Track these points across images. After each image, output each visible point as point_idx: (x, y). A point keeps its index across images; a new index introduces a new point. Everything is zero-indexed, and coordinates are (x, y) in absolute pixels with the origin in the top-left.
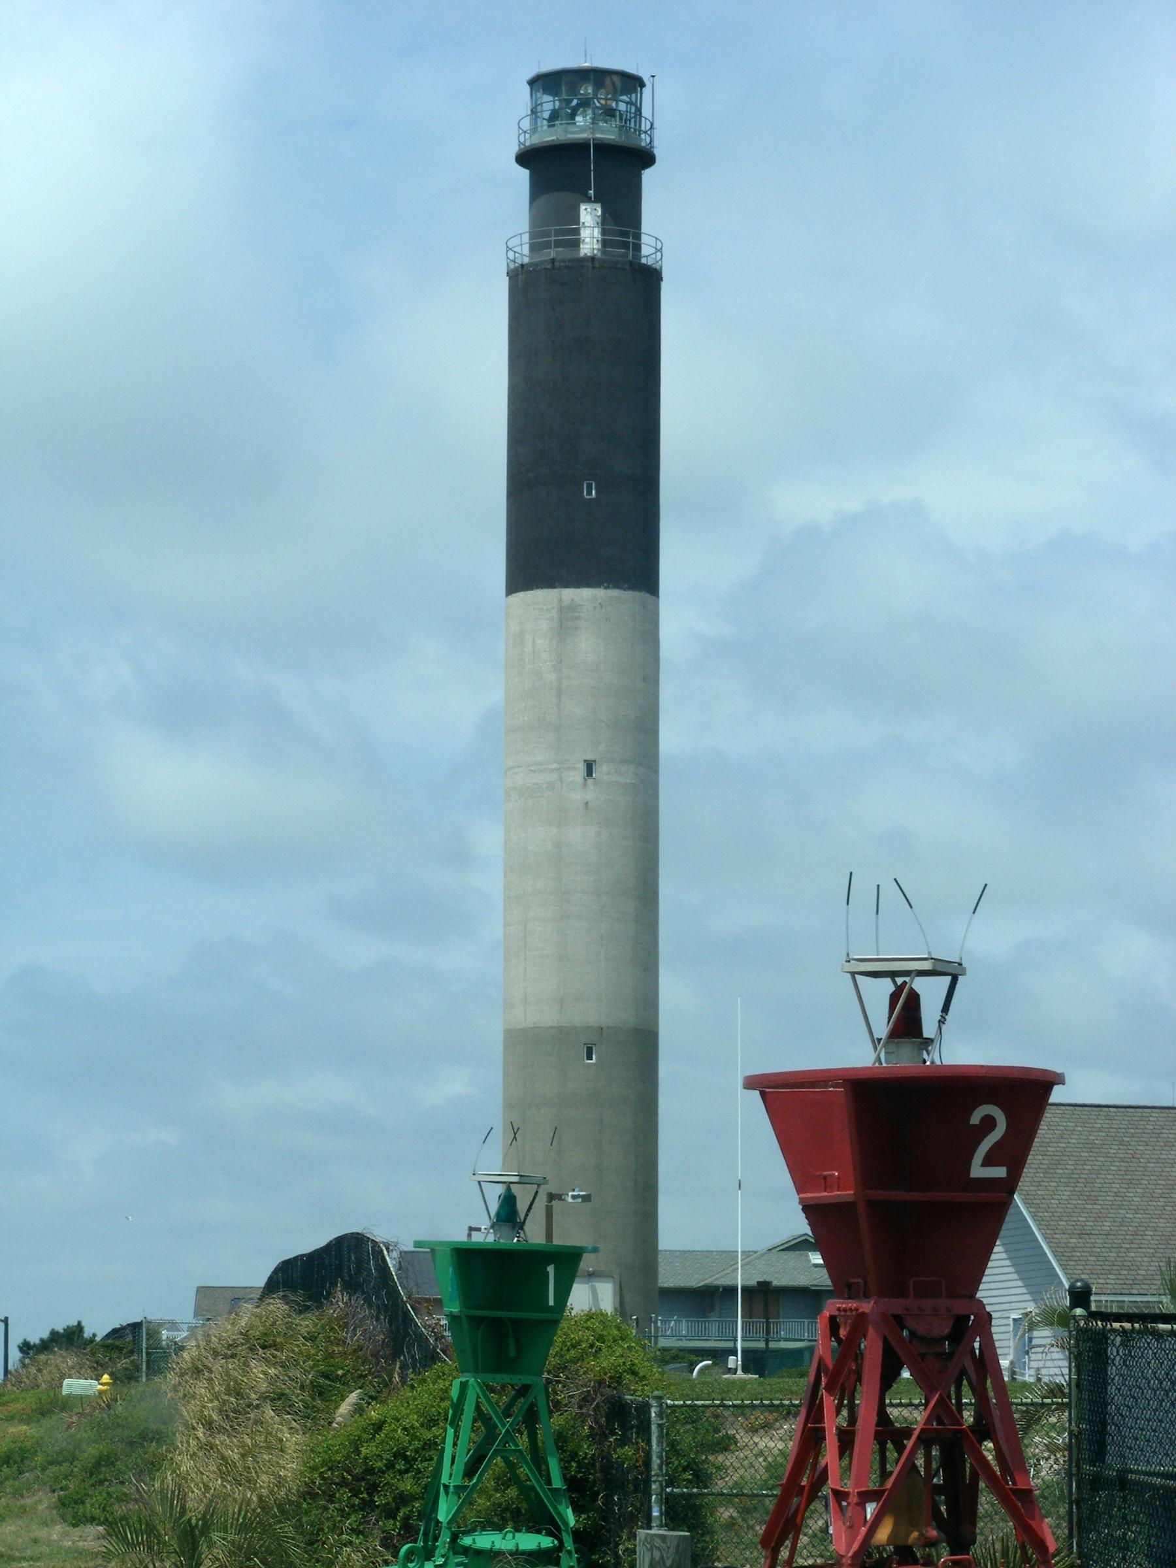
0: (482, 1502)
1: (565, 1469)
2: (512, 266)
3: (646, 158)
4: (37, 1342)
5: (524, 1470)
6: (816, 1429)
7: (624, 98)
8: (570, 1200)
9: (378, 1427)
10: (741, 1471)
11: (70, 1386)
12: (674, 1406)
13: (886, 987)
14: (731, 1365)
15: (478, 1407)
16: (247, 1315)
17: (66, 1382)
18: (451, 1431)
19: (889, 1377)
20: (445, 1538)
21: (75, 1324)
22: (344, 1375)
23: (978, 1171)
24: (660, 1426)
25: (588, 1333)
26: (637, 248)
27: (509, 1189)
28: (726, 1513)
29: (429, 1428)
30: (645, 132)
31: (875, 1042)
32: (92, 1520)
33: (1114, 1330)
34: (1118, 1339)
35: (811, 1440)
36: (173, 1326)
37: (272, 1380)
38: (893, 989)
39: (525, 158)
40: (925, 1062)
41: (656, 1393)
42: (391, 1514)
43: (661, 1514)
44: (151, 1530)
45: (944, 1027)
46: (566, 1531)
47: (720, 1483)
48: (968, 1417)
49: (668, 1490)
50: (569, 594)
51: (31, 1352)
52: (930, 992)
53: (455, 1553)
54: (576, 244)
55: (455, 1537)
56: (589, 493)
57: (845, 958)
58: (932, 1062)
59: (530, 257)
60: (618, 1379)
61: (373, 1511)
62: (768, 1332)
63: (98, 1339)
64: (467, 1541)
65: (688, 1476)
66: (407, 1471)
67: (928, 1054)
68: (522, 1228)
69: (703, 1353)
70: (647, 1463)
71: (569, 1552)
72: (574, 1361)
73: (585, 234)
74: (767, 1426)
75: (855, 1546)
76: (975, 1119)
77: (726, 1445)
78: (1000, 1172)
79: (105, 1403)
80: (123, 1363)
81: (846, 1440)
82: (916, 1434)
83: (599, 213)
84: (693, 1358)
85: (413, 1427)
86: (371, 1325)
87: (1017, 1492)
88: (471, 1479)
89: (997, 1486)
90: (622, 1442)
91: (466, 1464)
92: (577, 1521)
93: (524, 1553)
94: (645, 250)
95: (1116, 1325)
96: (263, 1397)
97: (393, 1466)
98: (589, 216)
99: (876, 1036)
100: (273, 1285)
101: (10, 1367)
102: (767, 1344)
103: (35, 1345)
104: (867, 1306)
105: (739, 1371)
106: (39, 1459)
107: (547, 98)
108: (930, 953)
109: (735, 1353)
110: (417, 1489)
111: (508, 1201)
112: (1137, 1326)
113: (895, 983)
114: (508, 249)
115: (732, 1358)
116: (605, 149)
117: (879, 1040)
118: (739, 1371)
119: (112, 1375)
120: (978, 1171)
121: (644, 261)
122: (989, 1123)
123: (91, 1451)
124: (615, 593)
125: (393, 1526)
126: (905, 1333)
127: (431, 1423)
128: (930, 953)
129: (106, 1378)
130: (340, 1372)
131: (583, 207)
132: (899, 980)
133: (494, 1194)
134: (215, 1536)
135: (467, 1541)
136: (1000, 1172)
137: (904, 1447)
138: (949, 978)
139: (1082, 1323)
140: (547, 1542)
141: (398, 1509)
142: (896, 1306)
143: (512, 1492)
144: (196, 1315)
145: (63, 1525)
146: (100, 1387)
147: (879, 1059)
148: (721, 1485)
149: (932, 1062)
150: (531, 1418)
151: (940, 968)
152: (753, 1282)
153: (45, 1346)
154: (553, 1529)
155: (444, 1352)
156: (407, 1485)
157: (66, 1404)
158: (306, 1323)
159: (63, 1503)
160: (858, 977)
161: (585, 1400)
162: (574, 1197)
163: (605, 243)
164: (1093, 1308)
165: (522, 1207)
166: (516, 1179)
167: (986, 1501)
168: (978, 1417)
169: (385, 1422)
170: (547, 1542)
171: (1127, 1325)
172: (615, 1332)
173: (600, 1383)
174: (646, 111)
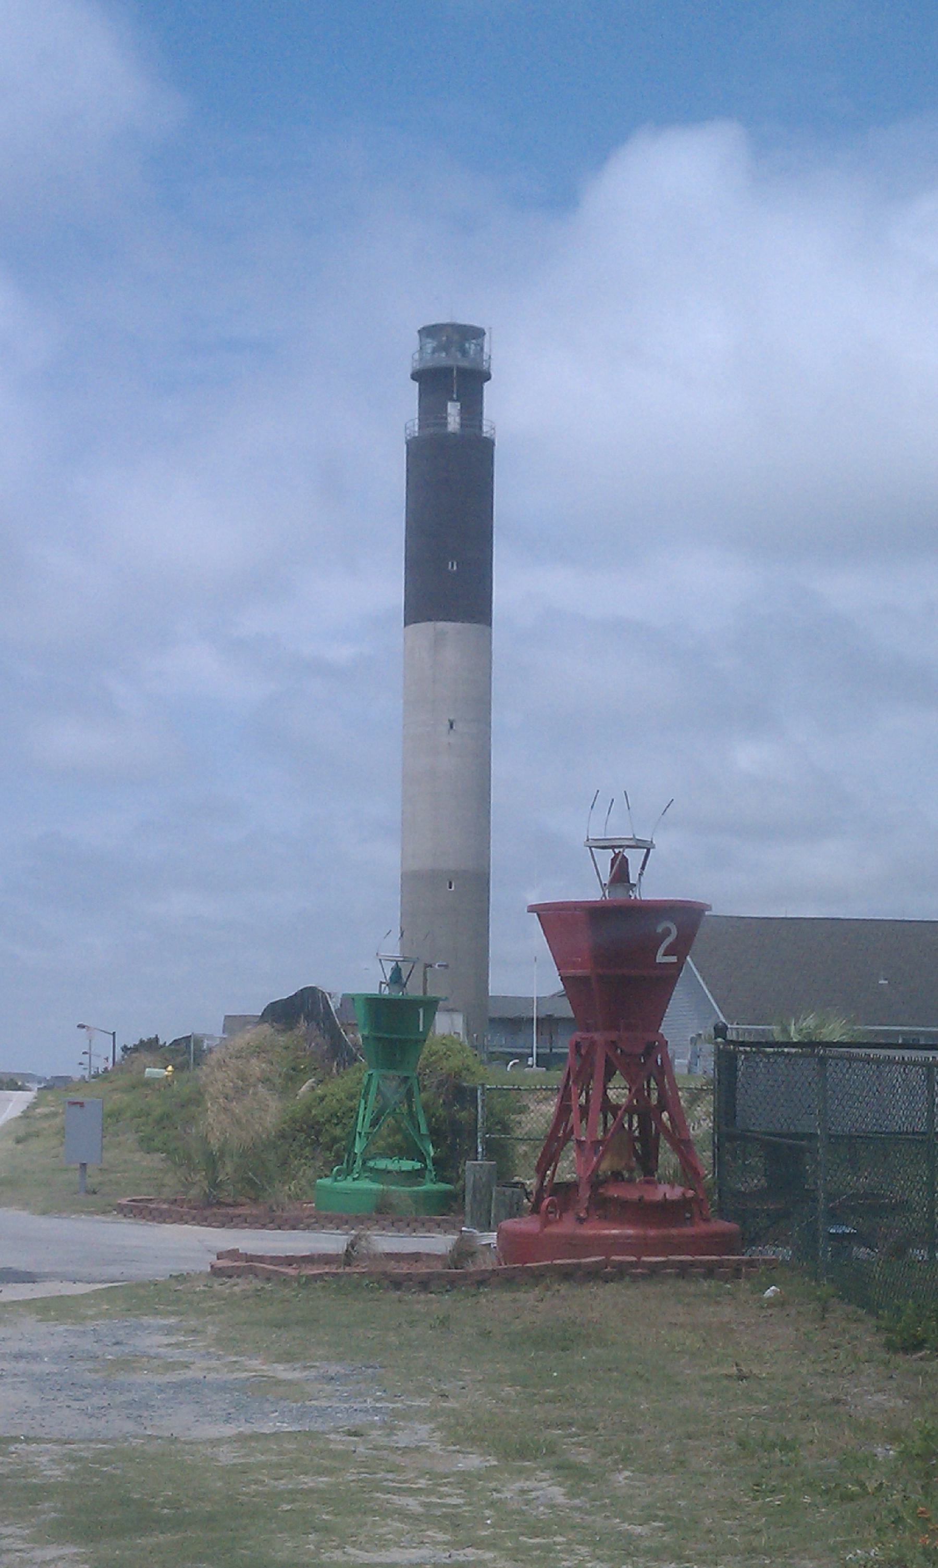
0: (381, 1143)
1: (429, 1124)
2: (408, 438)
3: (488, 377)
4: (132, 1046)
5: (405, 1124)
6: (568, 1105)
7: (474, 341)
8: (436, 967)
9: (322, 1099)
10: (529, 1125)
11: (149, 1072)
12: (491, 1089)
13: (610, 854)
14: (530, 1063)
15: (378, 1088)
16: (248, 1037)
17: (147, 1070)
18: (363, 1102)
19: (609, 1076)
20: (359, 1162)
21: (154, 1036)
22: (305, 1068)
23: (660, 959)
24: (483, 1101)
25: (443, 1047)
26: (481, 427)
27: (397, 964)
28: (522, 1148)
29: (352, 1101)
30: (486, 361)
31: (603, 886)
32: (157, 1150)
33: (741, 1052)
34: (743, 1057)
35: (564, 1111)
36: (211, 1037)
37: (263, 1071)
38: (613, 855)
39: (416, 376)
40: (631, 896)
41: (480, 1082)
42: (329, 1149)
43: (483, 1150)
44: (189, 1158)
45: (642, 878)
46: (429, 1158)
47: (518, 1132)
48: (654, 1100)
49: (488, 1136)
50: (441, 625)
51: (129, 1052)
52: (634, 857)
53: (365, 1171)
54: (445, 425)
55: (364, 1163)
56: (452, 566)
57: (586, 839)
58: (635, 898)
59: (419, 433)
60: (458, 1074)
61: (318, 1146)
62: (551, 1044)
63: (167, 1045)
64: (371, 1164)
65: (499, 1127)
66: (337, 1124)
67: (633, 891)
68: (405, 986)
69: (513, 1056)
70: (476, 1120)
71: (430, 1171)
72: (435, 1062)
73: (450, 419)
74: (546, 1099)
75: (589, 1173)
76: (659, 930)
77: (523, 1110)
78: (673, 959)
79: (167, 1083)
80: (180, 1059)
81: (584, 1111)
82: (623, 1108)
83: (459, 408)
84: (508, 1058)
85: (341, 1099)
86: (320, 1040)
87: (681, 1141)
88: (374, 1127)
89: (670, 1137)
90: (463, 1109)
91: (371, 1120)
92: (435, 1153)
93: (403, 1172)
94: (485, 429)
95: (741, 1048)
96: (259, 1080)
97: (330, 1121)
98: (453, 409)
99: (603, 882)
100: (263, 1018)
101: (116, 1060)
102: (551, 1050)
103: (131, 1048)
104: (597, 1036)
105: (535, 1066)
106: (128, 1114)
107: (429, 340)
108: (634, 836)
109: (532, 1056)
110: (344, 1134)
111: (397, 971)
112: (754, 1049)
113: (614, 852)
114: (406, 429)
115: (530, 1059)
116: (462, 372)
117: (605, 884)
118: (535, 1066)
119: (173, 1066)
120: (660, 959)
121: (484, 435)
122: (667, 932)
123: (157, 1112)
124: (467, 625)
125: (330, 1156)
126: (619, 1051)
127: (351, 1097)
128: (634, 836)
129: (170, 1068)
130: (302, 1067)
131: (450, 404)
132: (617, 851)
133: (389, 967)
134: (227, 1160)
135: (371, 1164)
136: (673, 959)
137: (617, 1115)
138: (645, 850)
139: (721, 1047)
140: (418, 1165)
141: (332, 1146)
142: (613, 1036)
143: (399, 1137)
144: (224, 1032)
145: (142, 1153)
146: (166, 1073)
147: (604, 895)
148: (518, 1133)
149: (635, 898)
150: (409, 1095)
151: (640, 844)
152: (542, 1015)
153: (136, 1049)
154: (421, 1158)
155: (361, 1056)
156: (338, 1132)
157: (147, 1083)
158: (282, 1039)
159: (142, 1140)
160: (593, 849)
161: (441, 1084)
162: (439, 966)
163: (462, 425)
164: (729, 1037)
165: (404, 974)
166: (401, 959)
167: (665, 1145)
168: (659, 1101)
169: (326, 1096)
170: (418, 1165)
171: (748, 1049)
172: (459, 1046)
173: (449, 1075)
174: (486, 349)
